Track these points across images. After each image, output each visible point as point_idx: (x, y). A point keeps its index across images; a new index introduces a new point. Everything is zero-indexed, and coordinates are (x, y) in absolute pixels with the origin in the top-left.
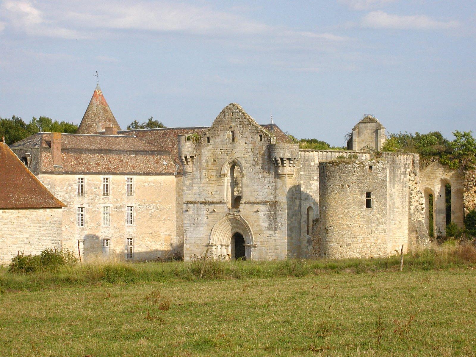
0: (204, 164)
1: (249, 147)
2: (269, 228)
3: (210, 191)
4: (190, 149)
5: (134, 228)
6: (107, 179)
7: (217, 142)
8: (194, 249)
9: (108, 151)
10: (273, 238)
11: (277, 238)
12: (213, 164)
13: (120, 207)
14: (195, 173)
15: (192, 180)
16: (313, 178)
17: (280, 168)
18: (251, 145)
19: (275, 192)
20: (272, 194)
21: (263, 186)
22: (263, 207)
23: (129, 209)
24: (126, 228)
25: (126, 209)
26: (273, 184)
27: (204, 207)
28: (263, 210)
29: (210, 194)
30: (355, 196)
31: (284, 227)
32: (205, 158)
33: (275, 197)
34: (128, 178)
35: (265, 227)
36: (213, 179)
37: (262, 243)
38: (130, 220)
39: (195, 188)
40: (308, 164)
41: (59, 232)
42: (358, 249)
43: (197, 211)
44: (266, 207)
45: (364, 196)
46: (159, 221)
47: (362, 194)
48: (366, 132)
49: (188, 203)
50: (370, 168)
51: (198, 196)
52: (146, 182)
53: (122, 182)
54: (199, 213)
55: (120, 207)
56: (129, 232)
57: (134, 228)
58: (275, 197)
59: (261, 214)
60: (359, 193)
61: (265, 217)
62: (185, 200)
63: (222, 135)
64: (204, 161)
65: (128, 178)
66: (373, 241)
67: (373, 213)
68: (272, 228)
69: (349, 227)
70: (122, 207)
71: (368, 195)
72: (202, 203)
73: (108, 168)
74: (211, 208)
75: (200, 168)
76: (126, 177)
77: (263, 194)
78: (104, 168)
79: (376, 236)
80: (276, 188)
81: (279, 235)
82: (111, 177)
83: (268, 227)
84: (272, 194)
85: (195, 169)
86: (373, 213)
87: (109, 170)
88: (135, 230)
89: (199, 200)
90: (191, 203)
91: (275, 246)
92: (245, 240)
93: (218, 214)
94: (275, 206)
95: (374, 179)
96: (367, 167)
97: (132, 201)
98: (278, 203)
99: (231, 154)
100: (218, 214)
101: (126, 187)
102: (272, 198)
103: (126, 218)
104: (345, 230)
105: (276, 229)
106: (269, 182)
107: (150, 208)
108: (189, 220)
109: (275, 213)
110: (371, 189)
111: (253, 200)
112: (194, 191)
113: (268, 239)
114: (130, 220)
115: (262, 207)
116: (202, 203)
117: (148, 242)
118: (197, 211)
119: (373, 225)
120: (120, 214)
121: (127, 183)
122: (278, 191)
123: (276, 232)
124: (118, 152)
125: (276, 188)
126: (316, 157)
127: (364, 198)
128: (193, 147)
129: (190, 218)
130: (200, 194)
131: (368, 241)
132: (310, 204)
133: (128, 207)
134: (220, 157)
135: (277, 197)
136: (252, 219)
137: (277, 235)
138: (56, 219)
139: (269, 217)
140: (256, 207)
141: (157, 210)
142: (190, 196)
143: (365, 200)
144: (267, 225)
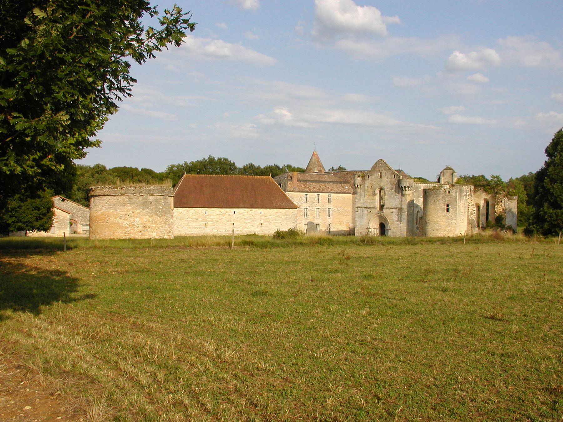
2: (398, 221)
27: (365, 210)
28: (395, 212)
38: (329, 215)
44: (397, 210)
49: (358, 207)
50: (449, 192)
59: (394, 214)
70: (325, 209)
71: (448, 206)
74: (369, 210)
80: (401, 201)
82: (321, 194)
97: (331, 206)
102: (399, 206)
115: (394, 210)
125: (401, 201)
127: (445, 207)
139: (398, 215)
140: (392, 210)
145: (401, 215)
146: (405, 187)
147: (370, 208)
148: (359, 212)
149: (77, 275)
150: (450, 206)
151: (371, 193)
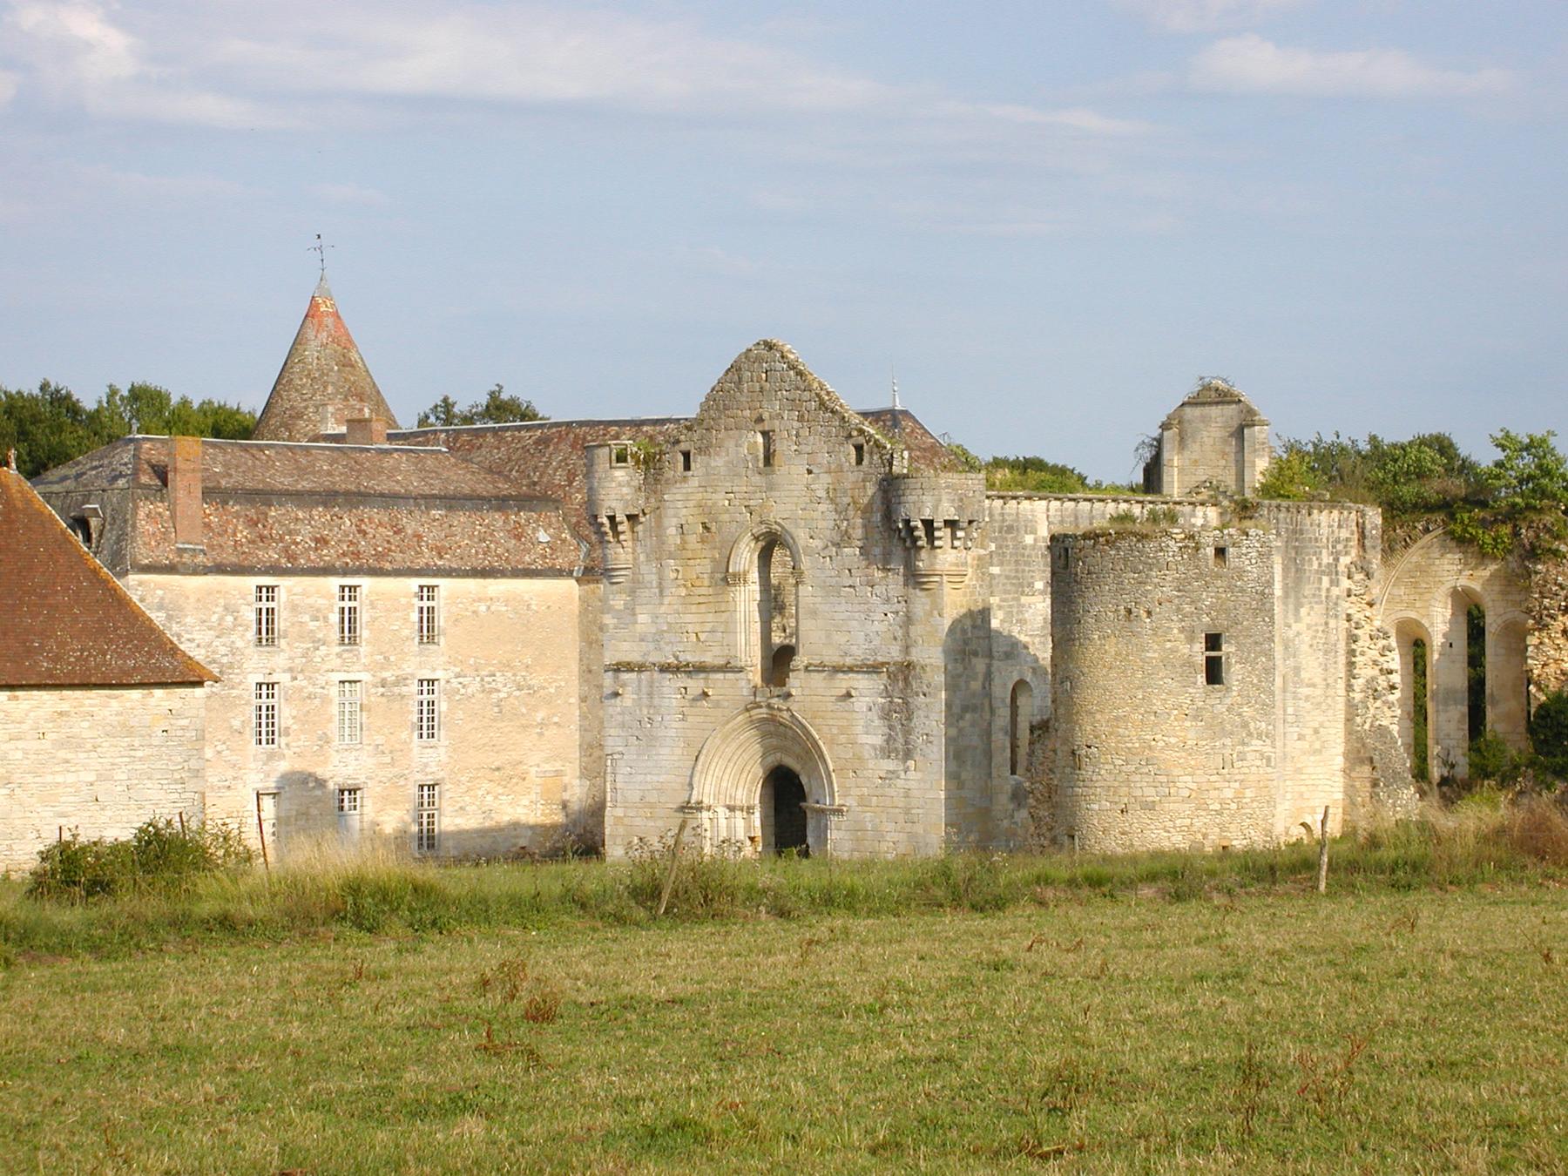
0: (671, 541)
2: (887, 751)
3: (690, 628)
4: (625, 490)
5: (442, 750)
6: (353, 588)
8: (638, 821)
10: (900, 783)
11: (913, 785)
12: (703, 541)
13: (397, 683)
14: (644, 569)
15: (632, 592)
16: (1031, 585)
17: (923, 554)
18: (826, 479)
19: (907, 634)
23: (425, 688)
24: (416, 750)
25: (415, 688)
28: (867, 689)
30: (1168, 645)
32: (674, 521)
33: (907, 649)
34: (421, 588)
35: (874, 747)
37: (863, 801)
38: (427, 725)
39: (642, 618)
40: (1014, 539)
41: (193, 764)
43: (650, 695)
44: (879, 682)
45: (1200, 646)
46: (525, 727)
47: (1191, 640)
49: (618, 668)
52: (480, 600)
53: (403, 601)
54: (656, 701)
55: (397, 683)
56: (426, 765)
57: (442, 750)
58: (907, 649)
59: (860, 704)
63: (730, 444)
64: (672, 531)
65: (421, 588)
66: (1229, 793)
67: (1228, 701)
70: (401, 681)
71: (1213, 641)
72: (665, 669)
73: (357, 555)
74: (695, 685)
75: (659, 554)
78: (344, 554)
80: (908, 620)
81: (919, 775)
82: (366, 583)
83: (882, 749)
85: (642, 558)
86: (1228, 701)
88: (444, 758)
89: (656, 657)
90: (629, 667)
93: (717, 705)
94: (906, 679)
95: (1230, 588)
96: (1210, 551)
101: (415, 617)
102: (894, 653)
103: (415, 717)
104: (1137, 759)
105: (908, 755)
106: (888, 601)
108: (623, 725)
110: (1221, 624)
111: (832, 658)
114: (427, 725)
115: (861, 682)
116: (665, 669)
117: (489, 798)
118: (650, 695)
119: (1228, 741)
120: (396, 706)
123: (911, 763)
124: (389, 499)
125: (908, 620)
128: (635, 483)
130: (658, 637)
131: (1214, 794)
135: (913, 650)
137: (912, 774)
138: (185, 722)
139: (886, 715)
140: (844, 682)
142: (625, 646)
143: (1201, 660)
144: (878, 740)
148: (628, 699)
150: (1227, 648)
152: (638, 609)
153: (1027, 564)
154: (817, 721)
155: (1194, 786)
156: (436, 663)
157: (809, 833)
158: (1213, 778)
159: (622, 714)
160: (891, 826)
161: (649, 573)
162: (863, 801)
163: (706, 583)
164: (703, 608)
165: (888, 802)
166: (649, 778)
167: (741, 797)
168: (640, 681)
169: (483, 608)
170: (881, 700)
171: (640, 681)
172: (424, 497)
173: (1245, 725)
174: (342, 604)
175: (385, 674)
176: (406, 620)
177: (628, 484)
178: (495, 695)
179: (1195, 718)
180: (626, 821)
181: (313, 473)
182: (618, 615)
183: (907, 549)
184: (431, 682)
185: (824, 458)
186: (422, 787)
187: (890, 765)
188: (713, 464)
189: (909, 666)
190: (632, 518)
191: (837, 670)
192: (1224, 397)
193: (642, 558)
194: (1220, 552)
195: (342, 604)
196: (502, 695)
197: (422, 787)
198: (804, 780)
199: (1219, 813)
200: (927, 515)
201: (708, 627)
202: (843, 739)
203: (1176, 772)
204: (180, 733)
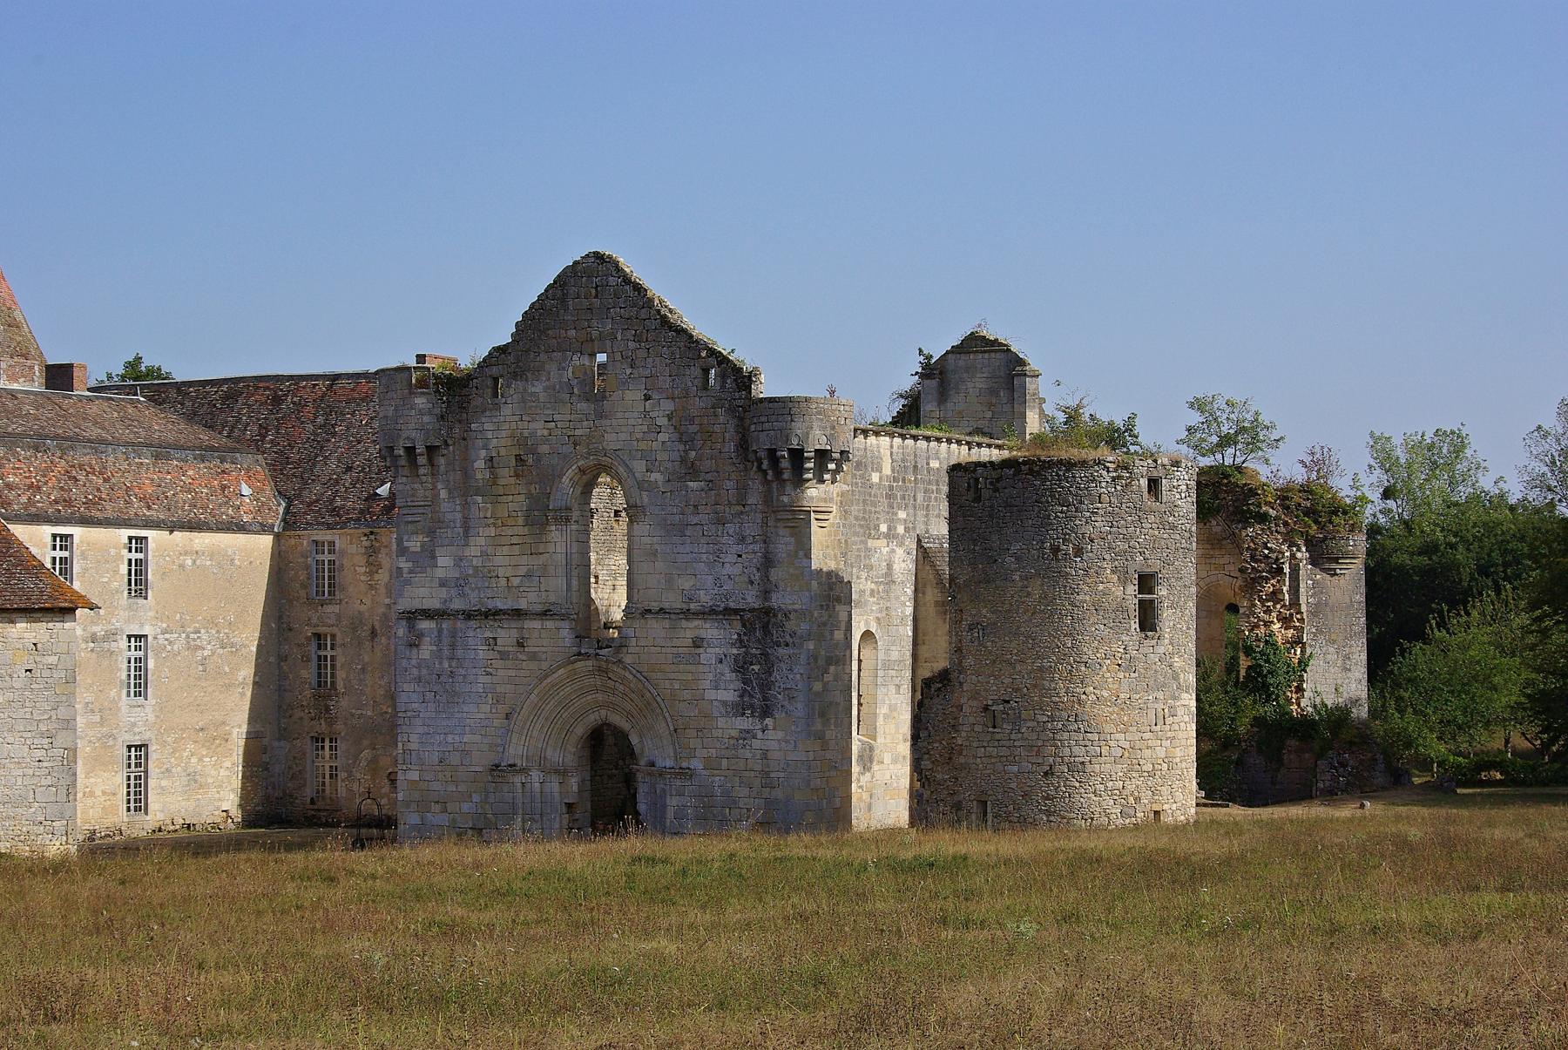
0: (479, 476)
1: (662, 410)
2: (740, 709)
3: (501, 572)
4: (426, 419)
5: (149, 710)
6: (64, 537)
7: (533, 394)
8: (436, 786)
9: (68, 442)
10: (756, 744)
11: (774, 745)
12: (517, 476)
13: (106, 638)
14: (445, 507)
15: (431, 533)
16: (877, 527)
17: (789, 488)
18: (668, 406)
19: (766, 577)
20: (752, 583)
21: (718, 553)
22: (715, 632)
23: (133, 644)
24: (124, 709)
25: (124, 643)
26: (757, 547)
27: (475, 635)
28: (719, 638)
29: (503, 582)
30: (1101, 587)
31: (800, 706)
32: (483, 453)
33: (766, 594)
34: (130, 538)
35: (724, 703)
36: (516, 530)
37: (710, 764)
38: (139, 684)
39: (441, 561)
40: (862, 477)
41: (63, 712)
42: (1110, 784)
43: (453, 646)
44: (734, 630)
45: (1132, 589)
46: (228, 686)
47: (1124, 582)
48: (970, 385)
49: (412, 616)
50: (1154, 484)
51: (453, 592)
52: (186, 553)
53: (113, 552)
54: (460, 653)
55: (106, 638)
56: (134, 725)
57: (149, 710)
58: (766, 594)
59: (709, 655)
60: (1115, 577)
61: (725, 668)
62: (405, 604)
63: (552, 367)
64: (480, 464)
65: (130, 538)
66: (1161, 752)
67: (1161, 650)
68: (752, 706)
69: (1079, 702)
70: (111, 635)
71: (1146, 582)
72: (468, 615)
73: (68, 503)
74: (506, 635)
75: (465, 489)
76: (125, 533)
77: (718, 582)
78: (56, 502)
79: (1169, 734)
80: (768, 562)
81: (780, 735)
82: (77, 532)
83: (735, 705)
84: (752, 583)
85: (443, 494)
86: (1161, 650)
87: (71, 506)
88: (151, 718)
89: (457, 605)
90: (427, 614)
91: (766, 774)
92: (637, 750)
93: (534, 657)
94: (765, 628)
95: (1163, 525)
96: (1144, 482)
97: (146, 618)
98: (775, 616)
99: (588, 436)
100: (534, 657)
101: (124, 569)
102: (751, 599)
103: (124, 676)
104: (1065, 714)
105: (766, 712)
106: (742, 540)
107: (198, 642)
108: (419, 680)
109: (765, 655)
110: (1155, 565)
111: (673, 601)
112: (440, 573)
113: (735, 748)
114: (139, 684)
115: (710, 631)
116: (468, 615)
117: (194, 760)
118: (453, 646)
119: (1160, 695)
120: (106, 662)
121: (128, 556)
122: (775, 575)
123: (768, 721)
124: (97, 445)
125: (768, 562)
126: (886, 453)
127: (1131, 593)
128: (437, 411)
129: (424, 671)
130: (460, 584)
131: (1147, 753)
132: (867, 623)
133: (129, 637)
134: (544, 449)
135: (774, 596)
136: (673, 676)
137: (770, 734)
138: (53, 659)
139: (741, 667)
140: (692, 628)
141: (221, 651)
142: (423, 592)
143: (1132, 604)
144: (730, 695)
145: (768, 664)
146: (410, 451)
147: (518, 614)
148: (426, 651)
149: (488, 634)
150: (1162, 591)
151: (517, 503)
152: (439, 551)
153: (874, 504)
154: (654, 675)
155: (1126, 745)
156: (146, 618)
157: (640, 797)
158: (1146, 736)
159: (419, 667)
160: (745, 791)
161: (449, 509)
162: (710, 764)
163: (521, 521)
164: (516, 550)
165: (742, 765)
166: (450, 739)
167: (554, 756)
168: (440, 631)
169: (189, 562)
170: (735, 651)
171: (440, 631)
172: (127, 444)
173: (1176, 677)
174: (54, 554)
175: (96, 629)
176: (116, 572)
177: (430, 413)
178: (199, 653)
179: (1128, 669)
180: (424, 785)
181: (20, 416)
182: (414, 558)
183: (766, 482)
184: (138, 637)
185: (665, 382)
186: (129, 747)
187: (744, 723)
188: (531, 389)
189: (768, 612)
190: (431, 450)
191: (687, 614)
192: (993, 346)
193: (443, 494)
194: (1154, 484)
195: (54, 554)
196: (206, 653)
197: (129, 747)
198: (634, 740)
199: (1152, 774)
200: (795, 444)
201: (522, 571)
202: (687, 695)
203: (1108, 728)
204: (46, 673)
